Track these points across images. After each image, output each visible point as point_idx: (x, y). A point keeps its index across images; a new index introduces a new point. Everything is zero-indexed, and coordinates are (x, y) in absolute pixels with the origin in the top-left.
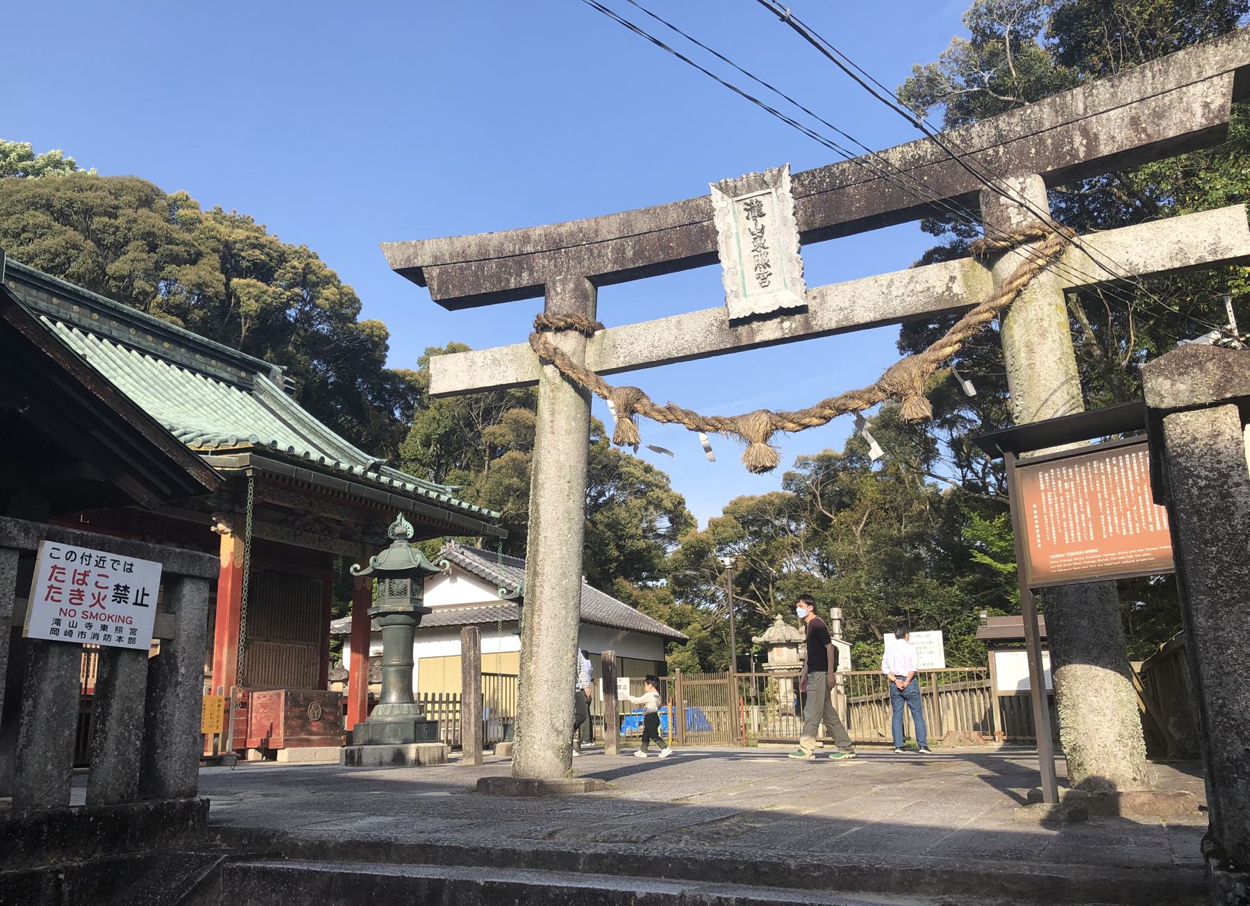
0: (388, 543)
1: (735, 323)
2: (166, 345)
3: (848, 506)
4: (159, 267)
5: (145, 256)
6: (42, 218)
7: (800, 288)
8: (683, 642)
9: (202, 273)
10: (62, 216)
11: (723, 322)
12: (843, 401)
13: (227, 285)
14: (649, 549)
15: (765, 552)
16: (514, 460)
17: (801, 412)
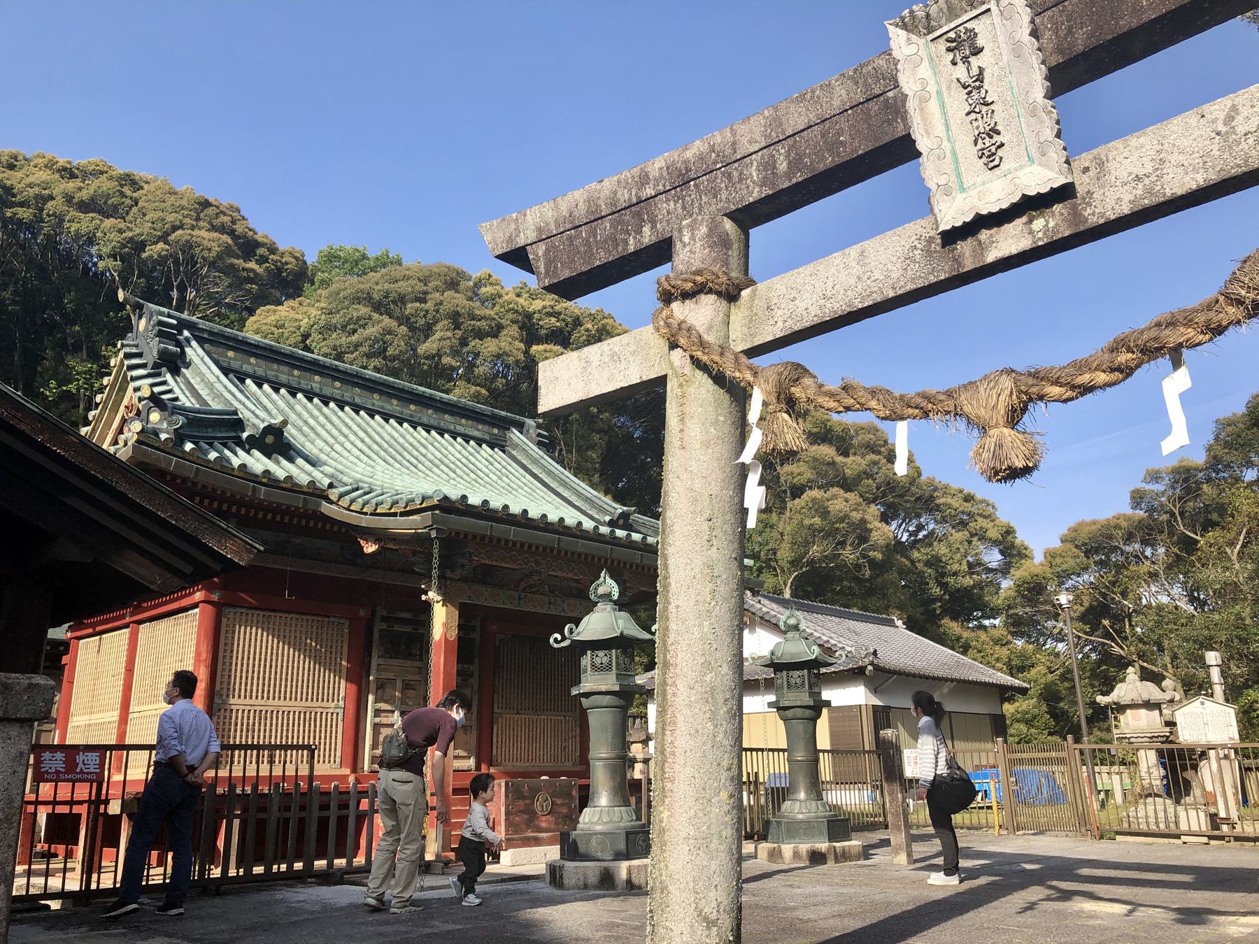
0: (590, 607)
1: (951, 237)
2: (412, 407)
3: (1217, 524)
4: (464, 342)
5: (449, 334)
6: (364, 310)
7: (1056, 154)
8: (1023, 692)
9: (503, 344)
10: (378, 307)
11: (930, 240)
12: (1154, 333)
13: (526, 352)
14: (980, 585)
15: (1113, 583)
16: (814, 500)
17: (1074, 364)
